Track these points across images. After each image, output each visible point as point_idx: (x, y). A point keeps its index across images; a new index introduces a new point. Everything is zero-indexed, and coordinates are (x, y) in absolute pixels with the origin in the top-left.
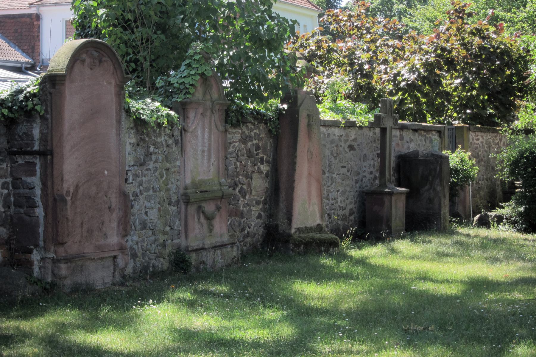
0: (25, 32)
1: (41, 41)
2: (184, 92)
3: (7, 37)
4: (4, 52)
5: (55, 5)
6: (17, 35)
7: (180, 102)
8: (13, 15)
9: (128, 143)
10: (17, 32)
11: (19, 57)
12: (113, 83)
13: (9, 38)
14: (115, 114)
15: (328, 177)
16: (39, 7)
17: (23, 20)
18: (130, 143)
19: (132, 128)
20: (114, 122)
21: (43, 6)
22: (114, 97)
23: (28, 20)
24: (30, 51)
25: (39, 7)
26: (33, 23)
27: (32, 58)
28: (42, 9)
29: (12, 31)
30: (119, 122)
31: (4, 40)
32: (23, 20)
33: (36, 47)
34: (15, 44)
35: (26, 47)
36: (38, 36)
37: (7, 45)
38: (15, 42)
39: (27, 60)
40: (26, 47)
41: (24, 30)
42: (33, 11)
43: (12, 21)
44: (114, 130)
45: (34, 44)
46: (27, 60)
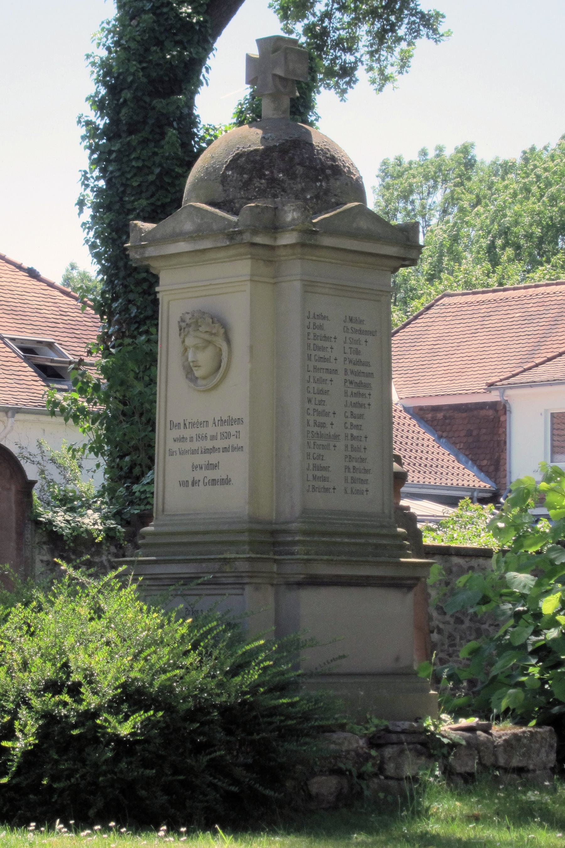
0: (484, 434)
1: (508, 451)
2: (145, 502)
3: (455, 443)
4: (444, 471)
5: (531, 386)
6: (470, 440)
7: (137, 514)
8: (466, 405)
9: (37, 560)
10: (471, 435)
11: (471, 479)
12: (13, 488)
13: (458, 446)
14: (14, 525)
15: (470, 628)
16: (505, 389)
17: (483, 413)
18: (42, 561)
19: (45, 543)
20: (14, 535)
21: (511, 388)
22: (13, 506)
23: (491, 413)
24: (492, 468)
25: (503, 389)
26: (499, 418)
27: (495, 482)
28: (509, 392)
29: (463, 434)
30: (20, 534)
31: (449, 449)
32: (483, 413)
33: (502, 462)
34: (467, 456)
35: (485, 462)
36: (505, 443)
37: (452, 457)
38: (467, 453)
39: (483, 484)
40: (485, 462)
41: (484, 431)
42: (494, 397)
43: (464, 415)
44: (13, 544)
45: (500, 456)
46: (483, 484)
